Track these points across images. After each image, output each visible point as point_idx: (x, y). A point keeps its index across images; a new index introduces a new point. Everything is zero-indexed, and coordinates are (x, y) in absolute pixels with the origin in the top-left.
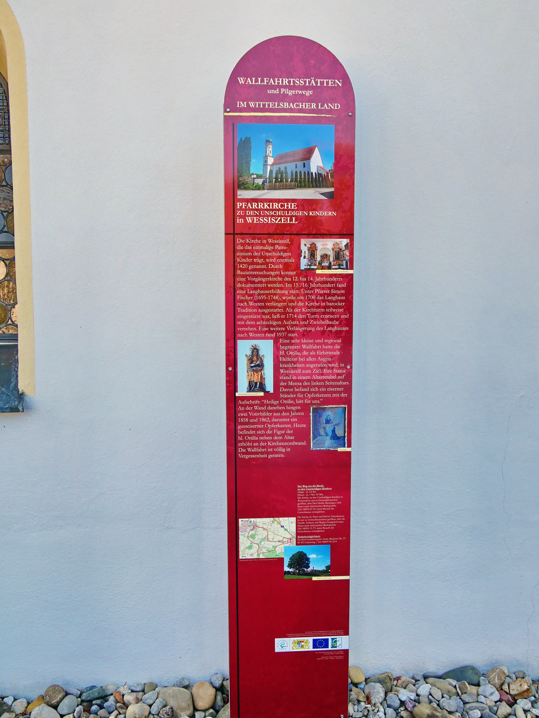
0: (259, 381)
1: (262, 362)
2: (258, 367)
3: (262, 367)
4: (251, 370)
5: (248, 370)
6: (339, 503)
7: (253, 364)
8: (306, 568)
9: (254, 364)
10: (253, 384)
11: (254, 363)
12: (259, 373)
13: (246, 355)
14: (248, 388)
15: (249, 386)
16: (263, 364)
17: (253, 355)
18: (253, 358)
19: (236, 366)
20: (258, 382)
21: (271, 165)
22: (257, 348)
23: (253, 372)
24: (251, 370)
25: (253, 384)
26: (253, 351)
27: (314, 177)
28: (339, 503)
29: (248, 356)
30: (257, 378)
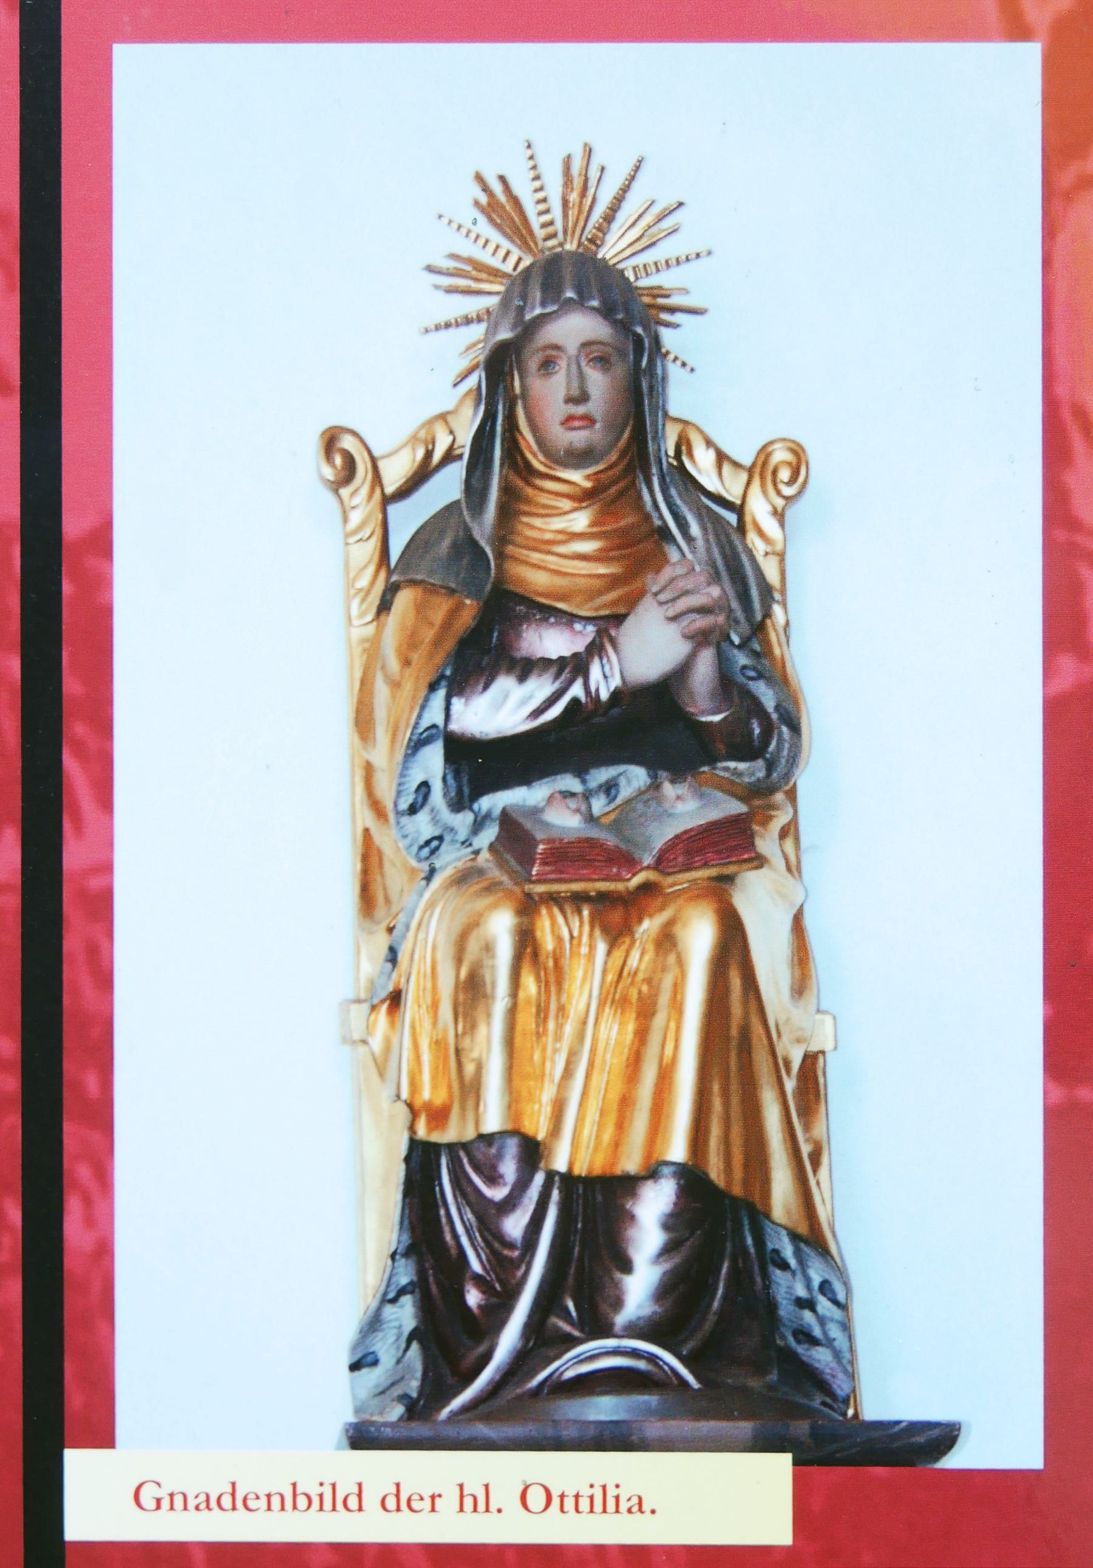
0: (677, 1150)
1: (759, 629)
2: (635, 777)
3: (750, 770)
4: (451, 859)
5: (386, 840)
6: (571, 1305)
7: (504, 683)
8: (536, 846)
9: (540, 688)
10: (514, 1226)
11: (525, 668)
12: (667, 940)
13: (330, 441)
14: (373, 1324)
15: (419, 1287)
16: (781, 680)
17: (513, 449)
18: (508, 513)
19: (76, 728)
20: (652, 1173)
21: (750, 471)
22: (608, 252)
23: (527, 908)
24: (451, 859)
25: (514, 1226)
26: (528, 330)
27: (752, 1250)
28: (571, 1305)
29: (394, 475)
30: (613, 1060)
